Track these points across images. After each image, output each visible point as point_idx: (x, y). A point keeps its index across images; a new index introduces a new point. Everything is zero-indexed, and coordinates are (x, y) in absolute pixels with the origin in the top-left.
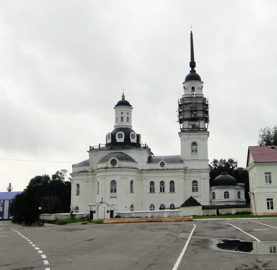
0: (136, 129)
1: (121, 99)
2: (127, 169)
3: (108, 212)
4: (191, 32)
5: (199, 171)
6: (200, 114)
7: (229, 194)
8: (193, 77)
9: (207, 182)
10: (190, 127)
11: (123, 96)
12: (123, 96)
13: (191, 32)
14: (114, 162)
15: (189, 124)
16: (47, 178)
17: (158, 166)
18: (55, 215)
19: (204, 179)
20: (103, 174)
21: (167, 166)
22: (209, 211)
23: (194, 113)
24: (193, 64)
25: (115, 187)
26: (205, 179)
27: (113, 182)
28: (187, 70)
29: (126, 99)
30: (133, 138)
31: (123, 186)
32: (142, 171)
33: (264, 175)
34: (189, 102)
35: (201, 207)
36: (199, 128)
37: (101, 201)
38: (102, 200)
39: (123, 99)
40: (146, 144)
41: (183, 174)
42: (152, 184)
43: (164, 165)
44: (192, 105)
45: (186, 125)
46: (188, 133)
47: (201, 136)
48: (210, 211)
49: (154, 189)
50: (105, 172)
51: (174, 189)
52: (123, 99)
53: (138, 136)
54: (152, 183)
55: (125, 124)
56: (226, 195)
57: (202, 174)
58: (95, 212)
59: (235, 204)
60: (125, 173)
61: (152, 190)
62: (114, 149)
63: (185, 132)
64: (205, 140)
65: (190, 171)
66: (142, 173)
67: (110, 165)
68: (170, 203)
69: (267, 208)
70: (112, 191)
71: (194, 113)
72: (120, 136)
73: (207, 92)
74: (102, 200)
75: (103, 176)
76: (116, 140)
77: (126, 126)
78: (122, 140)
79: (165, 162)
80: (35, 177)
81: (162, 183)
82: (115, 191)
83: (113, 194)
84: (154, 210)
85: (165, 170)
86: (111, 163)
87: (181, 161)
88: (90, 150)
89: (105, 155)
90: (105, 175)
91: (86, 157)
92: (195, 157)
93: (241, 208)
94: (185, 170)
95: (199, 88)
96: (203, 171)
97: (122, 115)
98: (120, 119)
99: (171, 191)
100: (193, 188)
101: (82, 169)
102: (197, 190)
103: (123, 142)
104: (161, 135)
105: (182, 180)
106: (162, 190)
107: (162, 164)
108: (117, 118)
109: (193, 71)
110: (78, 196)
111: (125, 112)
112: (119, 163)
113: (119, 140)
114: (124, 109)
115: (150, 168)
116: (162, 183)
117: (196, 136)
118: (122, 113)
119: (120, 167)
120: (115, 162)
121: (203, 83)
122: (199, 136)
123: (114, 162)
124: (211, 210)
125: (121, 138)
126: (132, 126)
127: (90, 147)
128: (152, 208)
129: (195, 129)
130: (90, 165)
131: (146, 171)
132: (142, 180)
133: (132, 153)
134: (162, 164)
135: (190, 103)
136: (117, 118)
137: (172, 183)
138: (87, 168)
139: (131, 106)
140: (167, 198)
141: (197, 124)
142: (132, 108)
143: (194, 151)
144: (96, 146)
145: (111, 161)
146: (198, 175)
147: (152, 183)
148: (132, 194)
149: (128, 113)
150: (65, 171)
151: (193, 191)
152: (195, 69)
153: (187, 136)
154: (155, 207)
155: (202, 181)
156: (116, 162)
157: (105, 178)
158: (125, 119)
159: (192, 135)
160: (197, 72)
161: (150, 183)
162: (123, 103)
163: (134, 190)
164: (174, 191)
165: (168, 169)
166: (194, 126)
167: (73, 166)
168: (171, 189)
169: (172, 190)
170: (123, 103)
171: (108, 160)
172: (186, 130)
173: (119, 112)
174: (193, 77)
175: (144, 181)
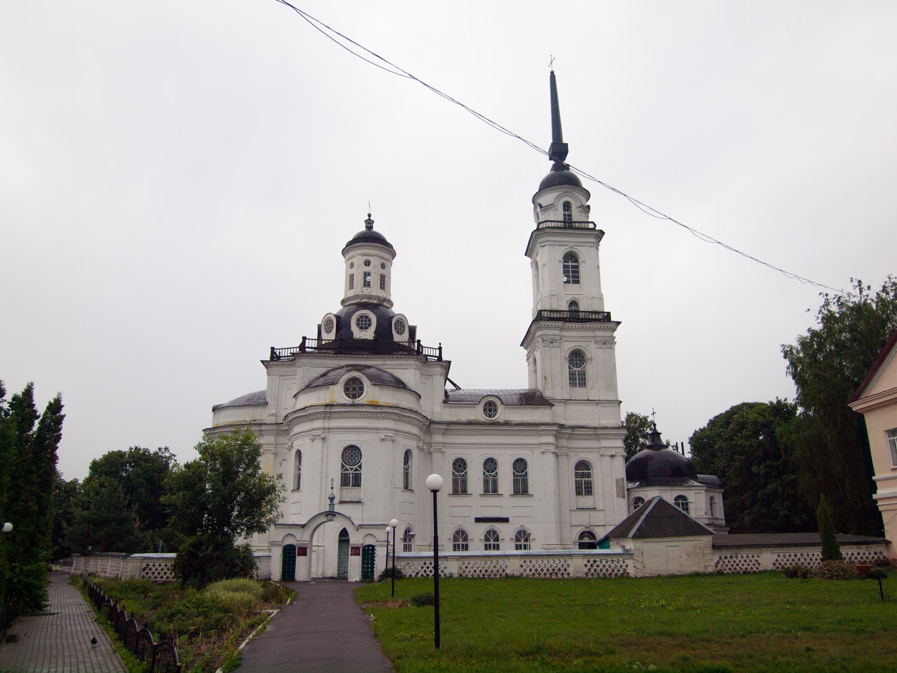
1: (363, 228)
2: (397, 411)
4: (552, 73)
5: (597, 432)
7: (687, 504)
8: (562, 179)
9: (619, 468)
11: (369, 223)
12: (369, 223)
13: (552, 73)
14: (354, 389)
17: (477, 414)
18: (145, 558)
19: (612, 456)
22: (737, 557)
24: (559, 151)
25: (356, 470)
26: (615, 458)
27: (352, 454)
28: (546, 167)
29: (376, 228)
30: (400, 332)
31: (380, 463)
32: (433, 426)
37: (328, 510)
38: (332, 504)
40: (440, 349)
41: (551, 439)
42: (460, 466)
43: (496, 410)
47: (598, 333)
48: (739, 556)
50: (324, 418)
53: (412, 331)
54: (460, 465)
55: (375, 291)
58: (303, 551)
64: (609, 343)
65: (569, 431)
66: (430, 431)
67: (344, 399)
69: (304, 557)
70: (345, 482)
72: (364, 323)
74: (332, 504)
75: (314, 433)
76: (352, 333)
77: (378, 298)
78: (369, 334)
79: (498, 403)
81: (490, 465)
82: (357, 482)
84: (467, 549)
88: (272, 358)
90: (324, 429)
92: (579, 393)
93: (854, 547)
96: (611, 434)
97: (367, 269)
98: (359, 280)
103: (367, 341)
105: (550, 458)
106: (491, 487)
107: (490, 408)
112: (371, 393)
113: (358, 334)
114: (371, 251)
116: (490, 465)
117: (582, 334)
118: (367, 263)
120: (357, 386)
122: (590, 334)
123: (353, 388)
125: (366, 328)
126: (392, 299)
127: (273, 349)
128: (461, 542)
131: (444, 427)
132: (431, 453)
133: (406, 371)
134: (490, 408)
137: (520, 465)
139: (389, 246)
143: (578, 379)
144: (289, 342)
145: (346, 384)
147: (460, 465)
148: (407, 495)
149: (383, 266)
151: (579, 493)
152: (567, 161)
154: (470, 537)
156: (362, 389)
157: (323, 439)
158: (374, 280)
161: (454, 464)
162: (369, 239)
163: (413, 485)
165: (506, 423)
167: (215, 409)
170: (369, 239)
173: (359, 261)
174: (562, 179)
175: (436, 456)
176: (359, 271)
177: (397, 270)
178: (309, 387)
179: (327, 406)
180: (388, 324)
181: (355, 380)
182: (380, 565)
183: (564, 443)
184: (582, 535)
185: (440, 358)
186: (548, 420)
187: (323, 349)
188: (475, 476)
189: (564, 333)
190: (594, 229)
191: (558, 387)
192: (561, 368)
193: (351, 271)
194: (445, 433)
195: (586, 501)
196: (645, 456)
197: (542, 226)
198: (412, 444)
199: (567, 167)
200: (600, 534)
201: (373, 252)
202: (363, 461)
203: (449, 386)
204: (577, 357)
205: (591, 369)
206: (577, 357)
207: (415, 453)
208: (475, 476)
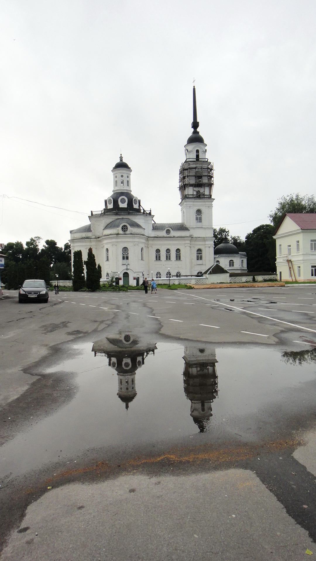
0: (135, 193)
1: (118, 161)
3: (135, 279)
5: (204, 239)
6: (205, 180)
8: (196, 139)
9: (212, 250)
10: (195, 193)
11: (121, 158)
12: (121, 158)
15: (194, 190)
16: (19, 245)
17: (163, 233)
20: (114, 240)
21: (173, 233)
23: (197, 179)
24: (195, 125)
27: (125, 249)
29: (124, 161)
33: (310, 242)
34: (194, 166)
35: (228, 274)
36: (204, 195)
39: (121, 160)
41: (189, 242)
44: (197, 170)
45: (190, 191)
46: (193, 200)
47: (206, 203)
49: (160, 257)
51: (180, 257)
52: (121, 160)
54: (158, 251)
55: (123, 188)
56: (231, 263)
57: (207, 243)
59: (240, 272)
60: (137, 240)
61: (158, 258)
62: (120, 215)
63: (188, 198)
64: (211, 207)
67: (121, 232)
68: (177, 271)
70: (124, 258)
71: (197, 179)
73: (210, 156)
76: (119, 205)
77: (127, 190)
80: (255, 231)
81: (168, 251)
82: (127, 258)
83: (125, 261)
85: (171, 237)
86: (122, 229)
87: (186, 229)
89: (111, 220)
91: (87, 222)
94: (191, 237)
95: (203, 151)
98: (119, 182)
99: (177, 259)
100: (198, 256)
101: (84, 235)
102: (201, 258)
103: (123, 208)
104: (163, 202)
105: (189, 248)
106: (168, 258)
107: (168, 232)
108: (116, 181)
109: (196, 132)
110: (107, 262)
111: (125, 176)
112: (130, 229)
113: (121, 205)
115: (156, 236)
116: (168, 251)
118: (122, 176)
119: (131, 234)
121: (206, 145)
122: (204, 203)
123: (124, 228)
124: (238, 278)
129: (199, 196)
130: (93, 231)
133: (138, 219)
134: (168, 232)
135: (195, 168)
136: (116, 181)
137: (178, 250)
138: (89, 234)
139: (129, 168)
140: (173, 266)
141: (202, 190)
142: (131, 171)
146: (203, 243)
147: (158, 251)
148: (142, 261)
149: (128, 177)
150: (39, 238)
151: (198, 259)
152: (198, 130)
153: (192, 203)
155: (207, 249)
156: (127, 228)
159: (197, 202)
160: (200, 134)
162: (121, 166)
163: (144, 259)
164: (180, 259)
165: (174, 237)
166: (198, 192)
168: (177, 256)
169: (178, 257)
170: (121, 166)
171: (118, 226)
172: (190, 196)
173: (119, 175)
174: (196, 139)
176: (119, 180)
177: (134, 177)
178: (106, 227)
179: (220, 283)
180: (131, 200)
181: (125, 226)
182: (141, 282)
183: (193, 243)
184: (198, 273)
185: (150, 214)
186: (188, 235)
187: (107, 211)
188: (163, 254)
189: (195, 203)
190: (207, 161)
191: (191, 222)
192: (194, 216)
193: (116, 179)
194: (153, 240)
195: (200, 262)
196: (222, 244)
197: (187, 160)
198: (143, 246)
199: (198, 133)
200: (203, 272)
201: (125, 172)
202: (129, 252)
203: (153, 222)
204: (199, 212)
205: (204, 216)
206: (199, 212)
207: (144, 248)
208: (163, 254)
